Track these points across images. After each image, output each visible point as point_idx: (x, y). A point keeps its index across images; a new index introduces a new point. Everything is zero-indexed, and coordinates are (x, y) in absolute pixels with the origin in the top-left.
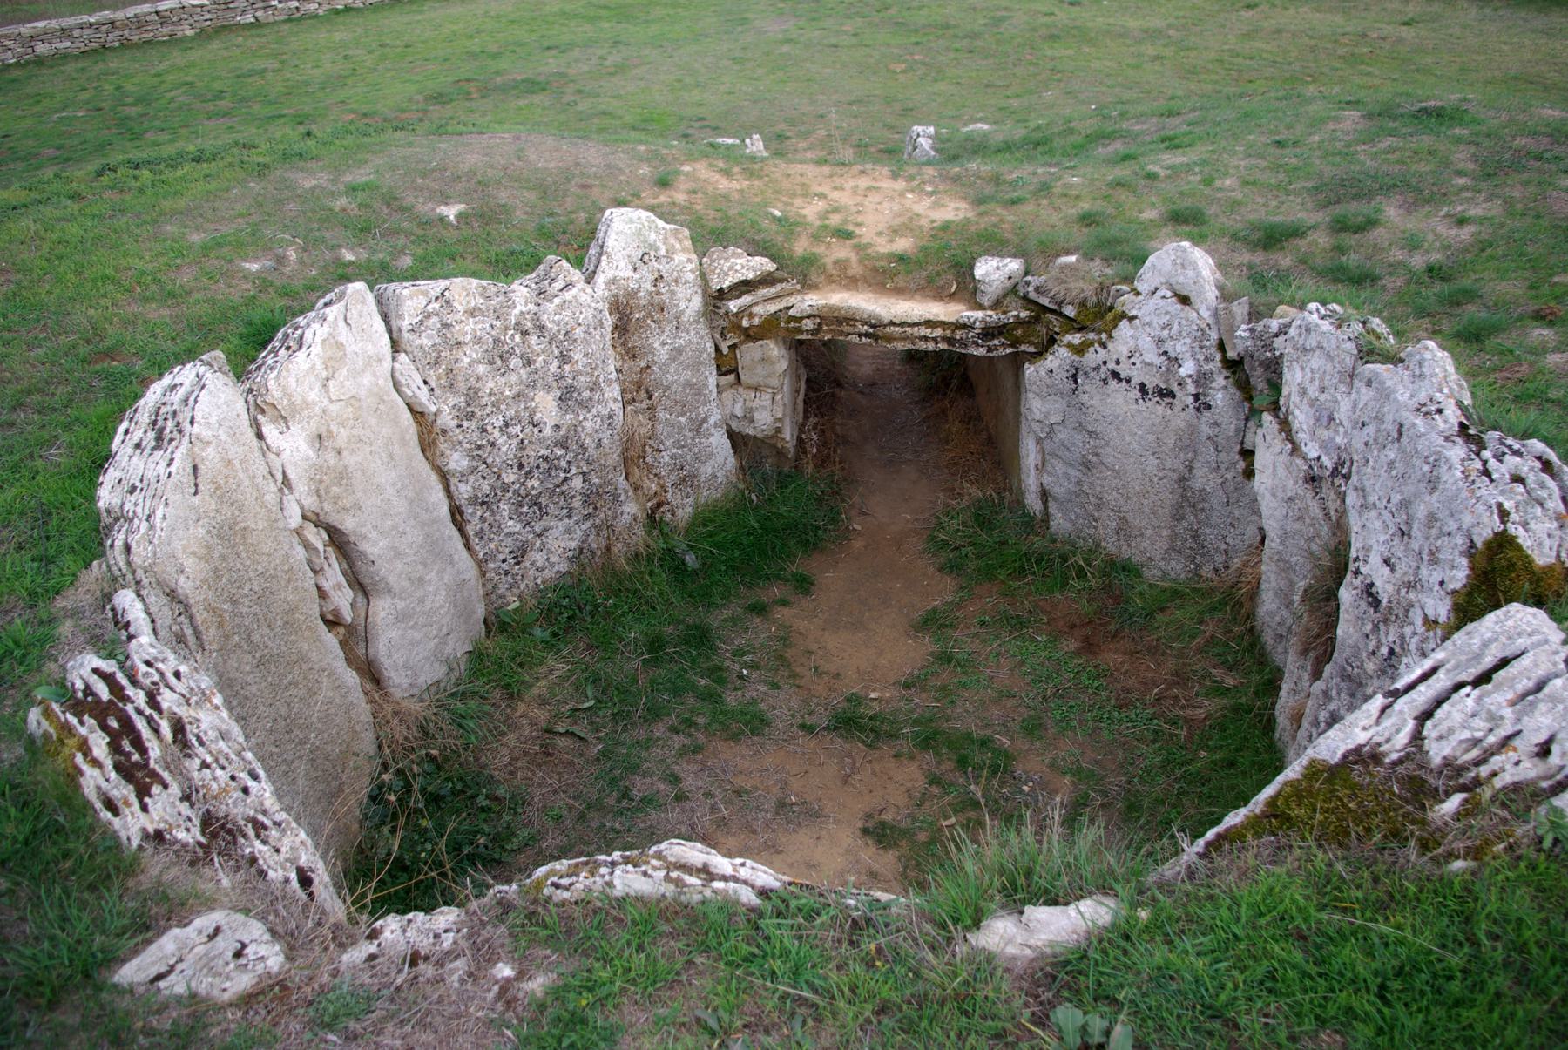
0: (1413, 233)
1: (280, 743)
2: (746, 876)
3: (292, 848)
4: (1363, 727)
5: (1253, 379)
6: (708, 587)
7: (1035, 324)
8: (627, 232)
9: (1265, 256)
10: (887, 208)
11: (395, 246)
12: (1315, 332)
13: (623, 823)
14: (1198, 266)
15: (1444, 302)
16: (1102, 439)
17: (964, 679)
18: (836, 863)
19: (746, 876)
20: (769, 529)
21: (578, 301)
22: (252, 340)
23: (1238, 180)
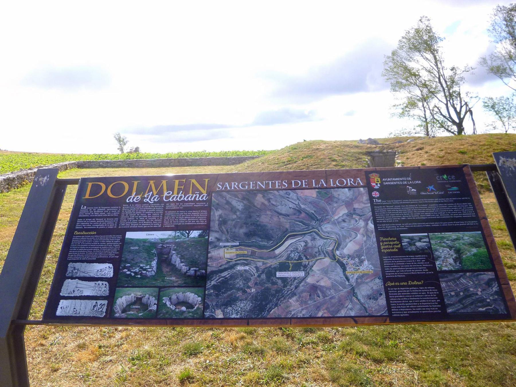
0: (154, 294)
1: (120, 309)
2: (133, 313)
3: (120, 312)
4: (151, 308)
5: (149, 299)
6: (461, 376)
7: (143, 297)
8: (132, 294)
9: (150, 295)
10: (139, 294)
11: (126, 295)
12: (151, 297)
13: (129, 311)
14: (147, 295)
15: (154, 296)
16: (144, 300)
17: (314, 375)
18: (135, 312)
19: (133, 313)
20: (134, 303)
21: (130, 296)
22: (121, 297)
23: (149, 293)
